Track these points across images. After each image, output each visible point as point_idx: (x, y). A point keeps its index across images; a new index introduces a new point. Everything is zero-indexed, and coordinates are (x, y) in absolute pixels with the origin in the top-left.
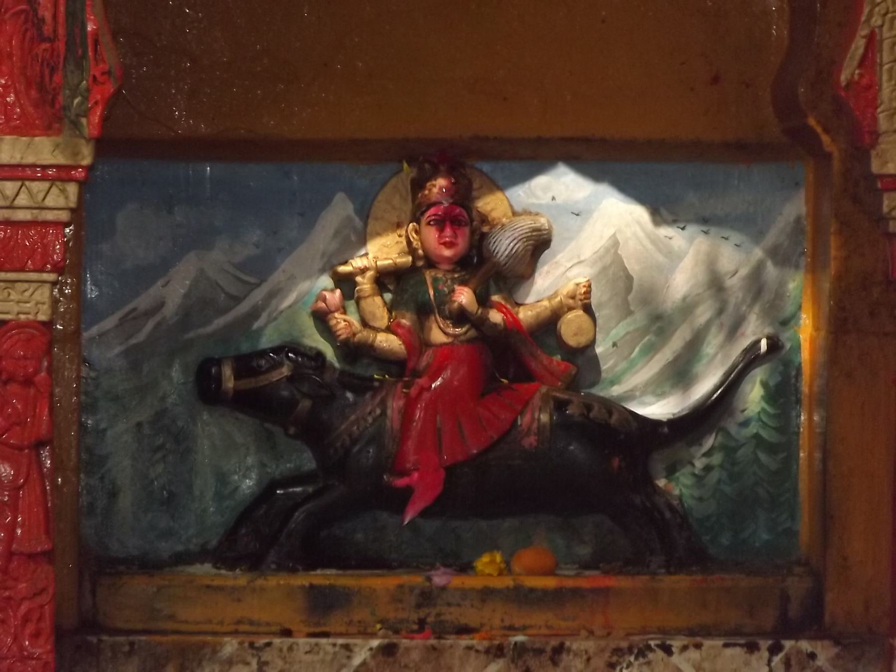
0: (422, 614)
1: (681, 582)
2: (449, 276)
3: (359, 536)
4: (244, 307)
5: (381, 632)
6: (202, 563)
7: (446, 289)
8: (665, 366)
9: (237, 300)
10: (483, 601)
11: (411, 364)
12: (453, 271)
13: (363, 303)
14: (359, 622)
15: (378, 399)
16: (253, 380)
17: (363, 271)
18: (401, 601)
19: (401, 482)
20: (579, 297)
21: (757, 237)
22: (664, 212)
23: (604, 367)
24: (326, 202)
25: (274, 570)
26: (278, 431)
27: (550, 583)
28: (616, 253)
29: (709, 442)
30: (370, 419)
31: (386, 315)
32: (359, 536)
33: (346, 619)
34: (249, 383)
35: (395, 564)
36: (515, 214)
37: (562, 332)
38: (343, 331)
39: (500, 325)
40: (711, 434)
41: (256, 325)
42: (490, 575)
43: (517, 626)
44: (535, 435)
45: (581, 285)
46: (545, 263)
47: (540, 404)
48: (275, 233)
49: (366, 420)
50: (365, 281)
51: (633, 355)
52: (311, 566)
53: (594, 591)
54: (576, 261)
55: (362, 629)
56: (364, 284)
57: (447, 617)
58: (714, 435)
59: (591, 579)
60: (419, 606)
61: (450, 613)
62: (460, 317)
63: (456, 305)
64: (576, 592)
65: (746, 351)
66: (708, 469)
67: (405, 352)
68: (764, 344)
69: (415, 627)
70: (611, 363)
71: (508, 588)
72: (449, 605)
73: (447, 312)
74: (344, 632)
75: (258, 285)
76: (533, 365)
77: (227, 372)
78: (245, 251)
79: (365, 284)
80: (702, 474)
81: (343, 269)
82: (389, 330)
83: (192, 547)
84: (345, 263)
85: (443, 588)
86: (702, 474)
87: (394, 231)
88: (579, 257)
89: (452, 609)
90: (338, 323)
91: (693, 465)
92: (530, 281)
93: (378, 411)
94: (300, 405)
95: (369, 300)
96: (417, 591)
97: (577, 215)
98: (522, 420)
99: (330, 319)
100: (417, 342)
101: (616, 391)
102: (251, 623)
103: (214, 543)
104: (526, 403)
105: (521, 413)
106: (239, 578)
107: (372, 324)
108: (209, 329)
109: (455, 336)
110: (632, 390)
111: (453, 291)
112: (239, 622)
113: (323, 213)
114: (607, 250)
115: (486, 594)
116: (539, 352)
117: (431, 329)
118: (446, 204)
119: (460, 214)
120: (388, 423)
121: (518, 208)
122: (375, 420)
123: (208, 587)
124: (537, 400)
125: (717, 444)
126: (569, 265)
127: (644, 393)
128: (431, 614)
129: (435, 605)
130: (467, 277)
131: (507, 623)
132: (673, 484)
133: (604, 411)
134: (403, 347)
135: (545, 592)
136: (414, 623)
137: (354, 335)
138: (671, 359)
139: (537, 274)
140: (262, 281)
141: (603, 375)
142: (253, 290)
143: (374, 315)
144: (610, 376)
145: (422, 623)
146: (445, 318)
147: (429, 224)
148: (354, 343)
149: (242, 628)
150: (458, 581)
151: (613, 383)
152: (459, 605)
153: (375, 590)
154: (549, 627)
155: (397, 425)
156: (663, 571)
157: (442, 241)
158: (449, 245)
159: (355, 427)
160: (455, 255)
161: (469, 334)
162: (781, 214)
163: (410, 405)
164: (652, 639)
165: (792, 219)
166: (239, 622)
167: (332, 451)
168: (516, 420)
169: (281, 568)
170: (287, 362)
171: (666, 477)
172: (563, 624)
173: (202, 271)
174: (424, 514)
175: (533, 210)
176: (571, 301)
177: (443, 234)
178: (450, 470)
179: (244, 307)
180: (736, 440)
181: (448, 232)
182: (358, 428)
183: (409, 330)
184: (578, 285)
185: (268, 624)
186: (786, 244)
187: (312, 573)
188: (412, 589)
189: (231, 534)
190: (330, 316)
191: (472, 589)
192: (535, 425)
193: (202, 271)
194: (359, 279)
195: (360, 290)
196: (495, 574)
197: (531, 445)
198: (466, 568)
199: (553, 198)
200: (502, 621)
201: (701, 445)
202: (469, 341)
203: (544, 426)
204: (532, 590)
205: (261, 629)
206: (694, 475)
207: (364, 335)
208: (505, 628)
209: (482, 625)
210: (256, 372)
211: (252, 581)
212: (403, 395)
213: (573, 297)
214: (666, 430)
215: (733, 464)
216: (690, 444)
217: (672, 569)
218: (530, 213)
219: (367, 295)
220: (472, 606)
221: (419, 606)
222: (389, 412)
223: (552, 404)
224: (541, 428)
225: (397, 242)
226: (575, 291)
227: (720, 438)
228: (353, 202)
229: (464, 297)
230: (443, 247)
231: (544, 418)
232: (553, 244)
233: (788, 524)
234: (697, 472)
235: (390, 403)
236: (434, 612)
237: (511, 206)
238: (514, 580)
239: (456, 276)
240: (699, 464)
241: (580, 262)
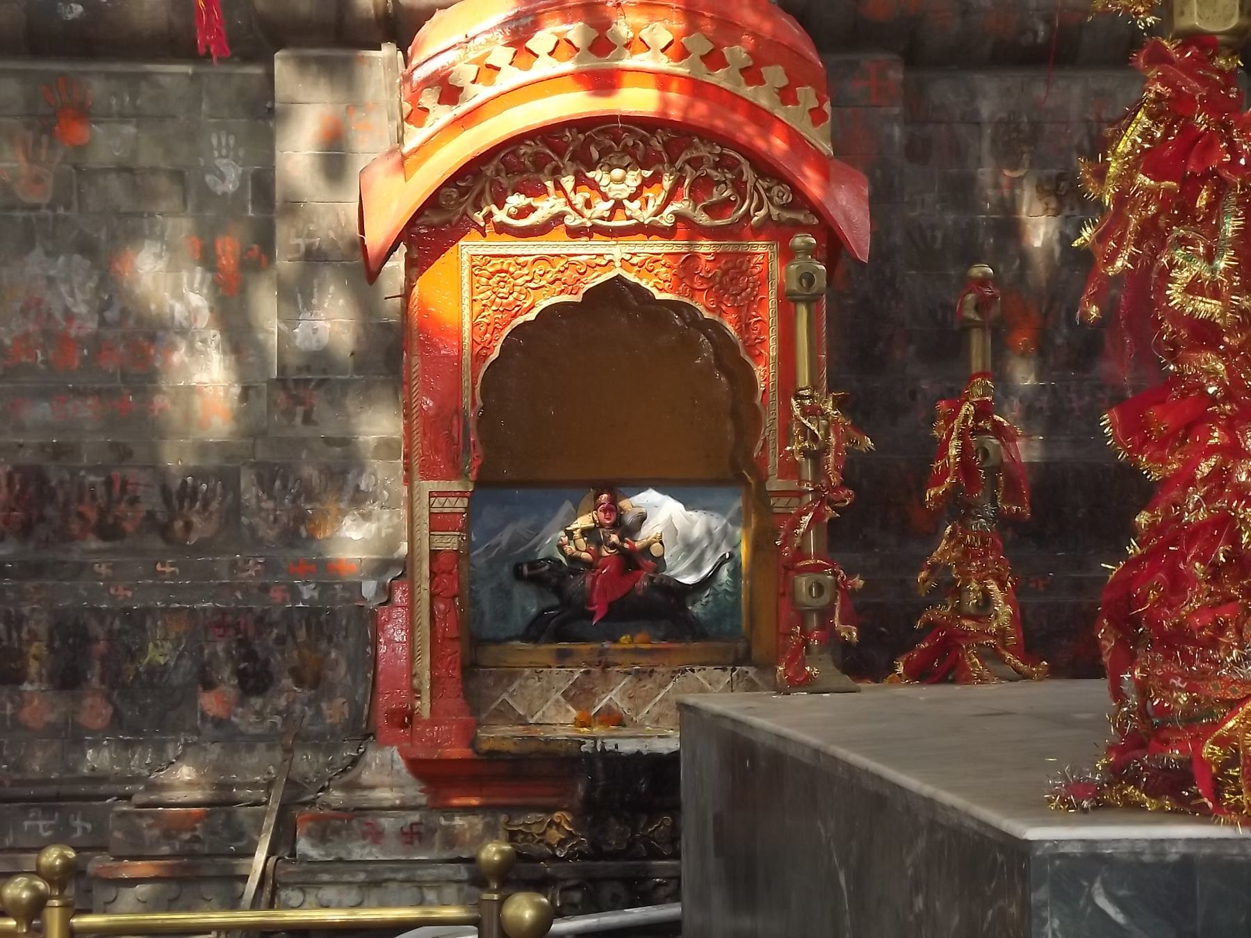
4: (531, 543)
9: (529, 541)
62: (613, 546)
79: (577, 534)
101: (672, 573)
115: (624, 651)
179: (531, 543)
198: (616, 641)
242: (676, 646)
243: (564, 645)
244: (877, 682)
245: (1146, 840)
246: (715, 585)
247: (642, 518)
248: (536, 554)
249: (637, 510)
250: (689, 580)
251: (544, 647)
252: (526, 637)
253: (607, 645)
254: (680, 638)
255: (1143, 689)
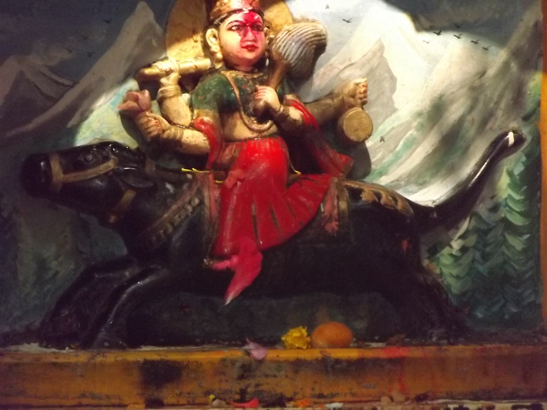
0: (242, 384)
1: (461, 350)
2: (249, 76)
3: (166, 316)
4: (60, 107)
5: (216, 403)
6: (29, 343)
7: (248, 89)
8: (425, 158)
9: (54, 101)
10: (296, 372)
11: (212, 159)
12: (252, 72)
13: (168, 103)
14: (189, 393)
15: (195, 188)
16: (81, 173)
17: (168, 73)
18: (224, 374)
19: (226, 264)
20: (359, 96)
21: (502, 42)
22: (422, 19)
23: (373, 160)
24: (131, 9)
25: (107, 347)
26: (94, 221)
27: (353, 354)
28: (381, 56)
29: (465, 226)
30: (190, 208)
31: (189, 114)
32: (166, 316)
33: (177, 391)
34: (72, 177)
35: (198, 340)
36: (295, 21)
37: (344, 127)
38: (154, 128)
39: (298, 121)
40: (465, 219)
41: (70, 124)
42: (299, 348)
43: (325, 394)
44: (336, 220)
45: (361, 85)
46: (321, 66)
47: (336, 192)
48: (85, 38)
49: (186, 209)
50: (170, 82)
51: (398, 149)
52: (134, 343)
53: (390, 360)
54: (347, 63)
55: (191, 400)
56: (169, 85)
57: (265, 388)
58: (468, 219)
59: (376, 350)
60: (241, 377)
61: (268, 384)
62: (265, 114)
63: (262, 103)
64: (376, 362)
65: (494, 143)
66: (464, 250)
67: (209, 147)
68: (511, 138)
69: (237, 397)
70: (379, 156)
71: (317, 359)
72: (267, 376)
73: (251, 110)
74: (176, 403)
75: (72, 87)
76: (322, 157)
77: (56, 167)
78: (60, 55)
79: (169, 84)
80: (459, 254)
81: (148, 71)
82: (192, 126)
83: (17, 327)
84: (149, 66)
85: (261, 362)
86: (459, 254)
87: (191, 37)
88: (350, 59)
89: (269, 380)
90: (149, 121)
91: (451, 247)
92: (309, 81)
93: (197, 201)
94: (125, 196)
95: (174, 100)
96: (238, 364)
97: (348, 22)
98: (324, 207)
99: (140, 118)
100: (220, 138)
101: (384, 181)
102: (93, 397)
103: (37, 323)
104: (325, 192)
105: (322, 200)
106: (69, 355)
107: (176, 121)
108: (30, 127)
109: (260, 132)
110: (397, 180)
111: (256, 90)
112: (83, 396)
113: (128, 20)
114: (374, 54)
115: (298, 365)
116: (327, 146)
117: (235, 125)
118: (246, 11)
119: (258, 21)
120: (207, 211)
121: (297, 16)
122: (194, 209)
123: (54, 364)
124: (334, 191)
125: (471, 228)
126: (342, 67)
127: (408, 183)
128: (251, 384)
129: (254, 377)
130: (265, 78)
131: (317, 392)
132: (434, 264)
133: (390, 198)
134: (207, 142)
135: (350, 362)
136: (237, 393)
137: (164, 131)
138: (430, 151)
139: (315, 76)
140: (75, 83)
141: (373, 167)
142: (67, 91)
143: (179, 113)
144: (378, 167)
145: (243, 392)
146: (249, 115)
147: (230, 29)
148: (163, 138)
149: (85, 401)
150: (271, 354)
151: (381, 174)
152: (275, 376)
153: (201, 364)
154: (353, 395)
155: (215, 213)
156: (445, 341)
157: (244, 45)
158: (251, 48)
159: (177, 216)
160: (255, 58)
161: (272, 129)
162: (521, 20)
163: (225, 193)
164: (450, 403)
165: (531, 24)
166: (83, 396)
167: (154, 238)
168: (319, 209)
169: (114, 346)
170: (113, 157)
171: (428, 258)
172: (364, 391)
173: (21, 74)
174: (244, 294)
175: (311, 18)
176: (352, 99)
177: (246, 38)
178: (267, 252)
179: (60, 107)
180: (487, 224)
181: (250, 35)
182: (180, 217)
183: (212, 127)
184: (357, 84)
185: (108, 397)
186: (527, 47)
187: (138, 349)
188: (233, 362)
189: (54, 315)
190: (141, 115)
191: (287, 361)
192: (336, 212)
193: (21, 74)
194: (163, 80)
195: (166, 91)
196: (305, 347)
197: (333, 229)
198: (272, 342)
199: (327, 7)
200: (313, 389)
201: (458, 229)
202: (271, 136)
203: (343, 212)
204: (338, 361)
205: (104, 402)
206: (452, 255)
207: (172, 131)
208: (313, 396)
209: (295, 394)
210: (80, 166)
211: (93, 358)
212: (217, 186)
213: (353, 96)
214: (435, 215)
215: (486, 245)
216: (448, 228)
217: (452, 340)
218: (308, 20)
219: (172, 95)
220: (287, 376)
221: (241, 377)
222: (207, 201)
223: (346, 193)
224: (341, 214)
225: (193, 47)
226: (355, 90)
227: (473, 222)
228: (154, 11)
229: (268, 95)
230: (245, 50)
231: (343, 205)
232: (328, 48)
233: (532, 298)
234: (454, 253)
235: (206, 194)
236: (253, 382)
237: (291, 14)
238: (321, 352)
239: (255, 76)
240: (456, 245)
241: (351, 65)
242: (415, 352)
243: (149, 353)
244: (420, 27)
245: (540, 154)
246: (482, 209)
247: (318, 46)
248: (73, 132)
249: (307, 29)
250: (432, 194)
251: (112, 357)
252: (52, 334)
253: (258, 353)
254: (416, 334)
255: (198, 115)
